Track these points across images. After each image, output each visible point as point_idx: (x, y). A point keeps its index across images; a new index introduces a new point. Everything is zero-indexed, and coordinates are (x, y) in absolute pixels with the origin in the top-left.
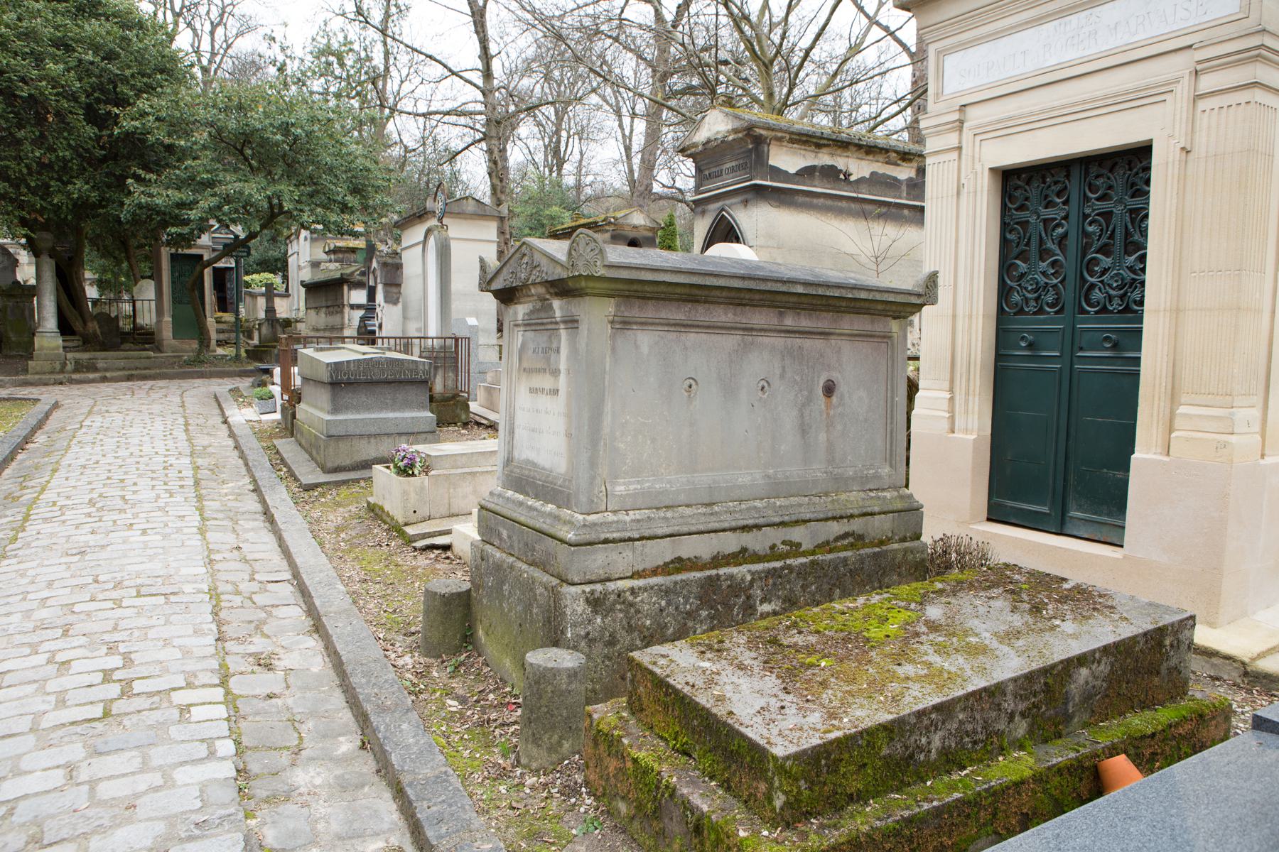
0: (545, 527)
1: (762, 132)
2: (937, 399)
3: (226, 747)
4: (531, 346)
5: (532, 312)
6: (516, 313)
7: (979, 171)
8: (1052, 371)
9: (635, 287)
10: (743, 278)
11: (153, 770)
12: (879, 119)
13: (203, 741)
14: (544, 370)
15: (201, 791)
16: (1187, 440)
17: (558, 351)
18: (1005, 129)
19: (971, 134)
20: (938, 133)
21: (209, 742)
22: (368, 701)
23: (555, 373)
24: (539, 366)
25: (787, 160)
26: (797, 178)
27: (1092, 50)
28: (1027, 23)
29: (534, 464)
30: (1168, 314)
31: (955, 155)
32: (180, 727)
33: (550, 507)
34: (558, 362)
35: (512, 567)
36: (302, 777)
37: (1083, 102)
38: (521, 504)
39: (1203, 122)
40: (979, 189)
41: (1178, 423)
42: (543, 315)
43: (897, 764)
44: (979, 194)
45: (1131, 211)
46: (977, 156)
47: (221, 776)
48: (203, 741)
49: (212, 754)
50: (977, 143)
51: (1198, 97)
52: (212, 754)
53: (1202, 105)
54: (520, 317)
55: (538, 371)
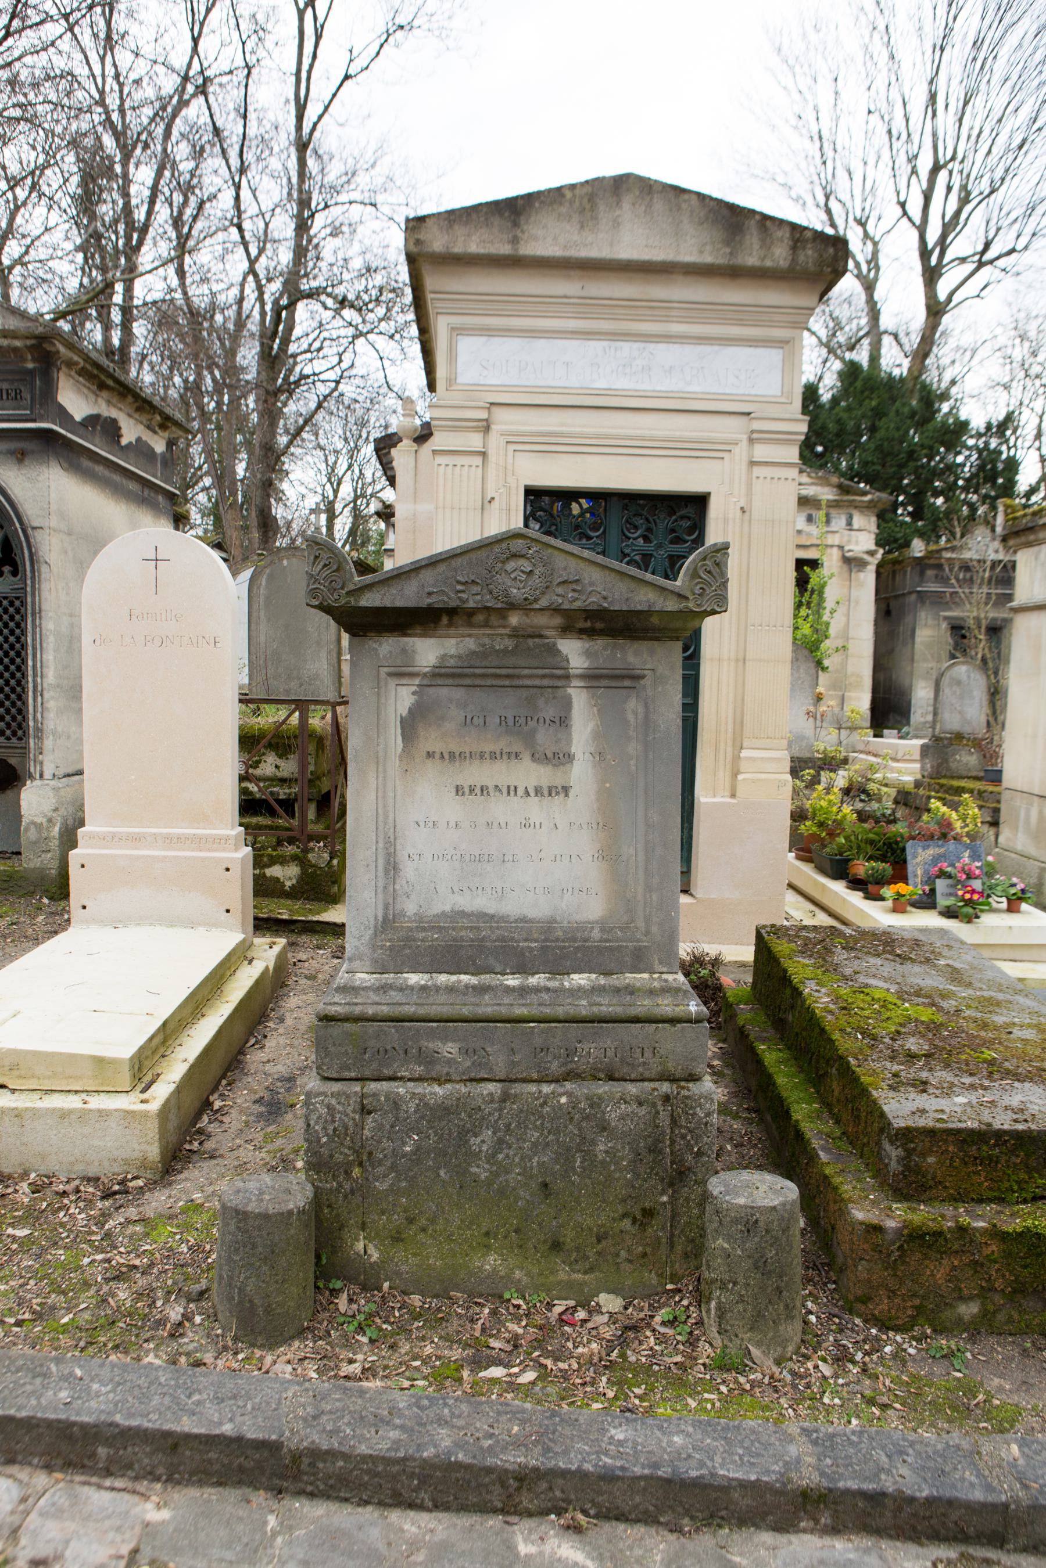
1: (62, 349)
7: (514, 485)
9: (497, 549)
10: (31, 555)
16: (753, 781)
18: (547, 445)
19: (503, 440)
20: (454, 429)
25: (75, 401)
26: (82, 430)
27: (645, 386)
28: (572, 332)
30: (733, 664)
31: (478, 460)
35: (459, 982)
37: (598, 437)
39: (758, 487)
40: (513, 507)
41: (743, 766)
43: (896, 1135)
44: (513, 513)
45: (671, 557)
46: (510, 467)
50: (510, 453)
51: (753, 463)
53: (757, 471)
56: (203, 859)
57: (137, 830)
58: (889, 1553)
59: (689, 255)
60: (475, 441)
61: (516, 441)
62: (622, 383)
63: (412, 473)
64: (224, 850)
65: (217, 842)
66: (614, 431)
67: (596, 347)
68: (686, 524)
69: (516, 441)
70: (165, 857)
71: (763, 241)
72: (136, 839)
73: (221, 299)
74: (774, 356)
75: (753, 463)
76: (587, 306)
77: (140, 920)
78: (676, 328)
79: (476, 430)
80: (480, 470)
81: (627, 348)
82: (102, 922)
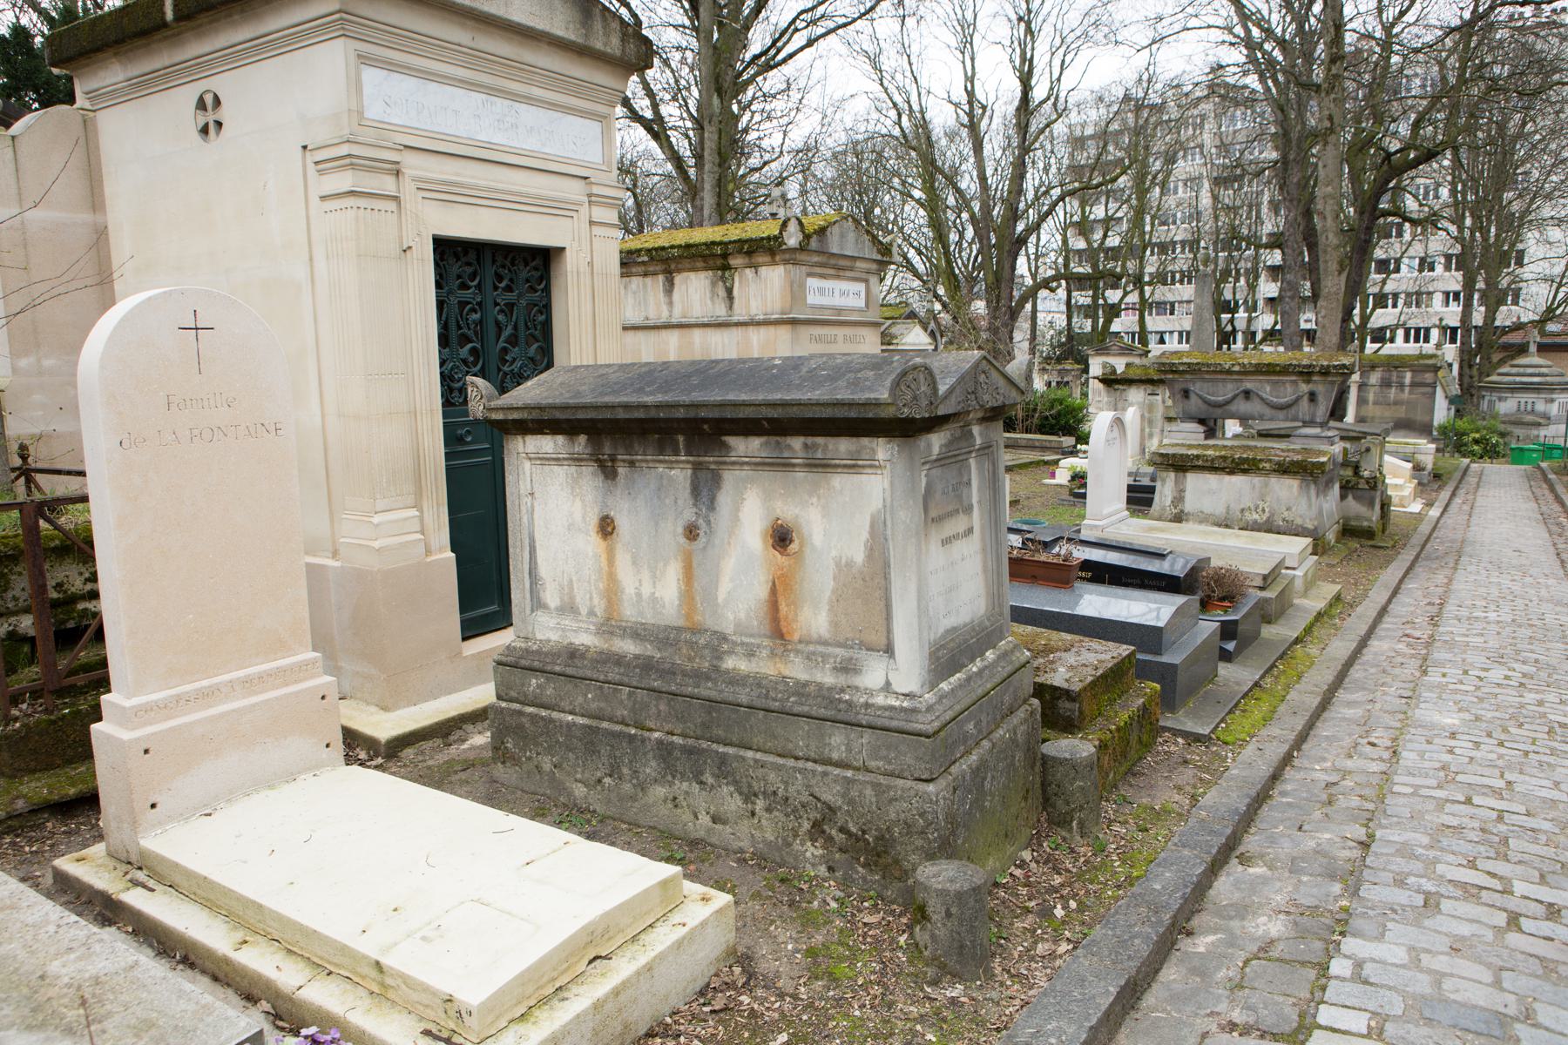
0: (1009, 669)
2: (406, 519)
3: (1339, 967)
4: (939, 487)
5: (950, 443)
6: (929, 446)
8: (485, 464)
11: (1430, 971)
12: (833, 261)
13: (1366, 982)
14: (957, 511)
15: (1383, 935)
17: (969, 483)
18: (448, 194)
21: (1359, 978)
22: (1160, 922)
23: (968, 509)
24: (950, 508)
29: (954, 629)
31: (392, 206)
32: (1387, 1010)
33: (990, 655)
34: (970, 497)
36: (1275, 927)
37: (489, 189)
38: (969, 679)
42: (964, 444)
47: (1359, 941)
48: (1366, 982)
49: (1359, 965)
52: (1359, 965)
53: (597, 230)
54: (936, 450)
55: (950, 514)
56: (297, 694)
57: (205, 683)
58: (1333, 715)
59: (559, 32)
60: (387, 184)
61: (427, 188)
62: (499, 138)
63: (12, 166)
64: (313, 677)
65: (301, 671)
66: (500, 186)
67: (478, 97)
68: (469, 270)
69: (427, 188)
70: (254, 705)
71: (604, 28)
72: (206, 696)
73: (765, 144)
74: (594, 127)
75: (591, 223)
76: (476, 58)
77: (231, 794)
78: (537, 92)
79: (388, 172)
80: (395, 216)
81: (500, 104)
82: (183, 816)
